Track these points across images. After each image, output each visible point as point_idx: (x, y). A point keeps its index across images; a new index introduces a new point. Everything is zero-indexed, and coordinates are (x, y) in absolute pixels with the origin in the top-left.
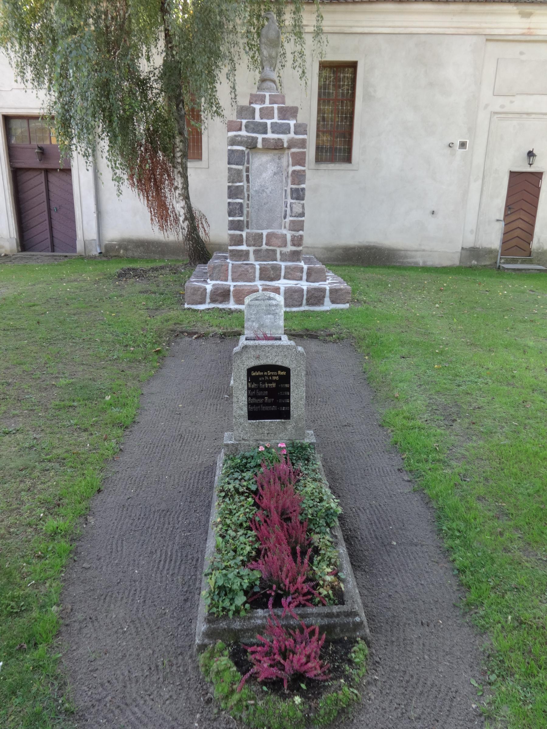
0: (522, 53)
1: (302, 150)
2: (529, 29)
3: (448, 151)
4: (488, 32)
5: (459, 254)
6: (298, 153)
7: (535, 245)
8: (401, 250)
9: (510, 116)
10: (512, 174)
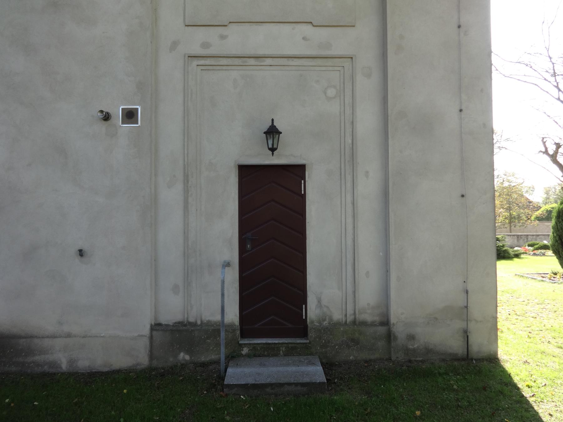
3: (102, 127)
5: (146, 341)
7: (312, 311)
8: (20, 337)
10: (247, 173)
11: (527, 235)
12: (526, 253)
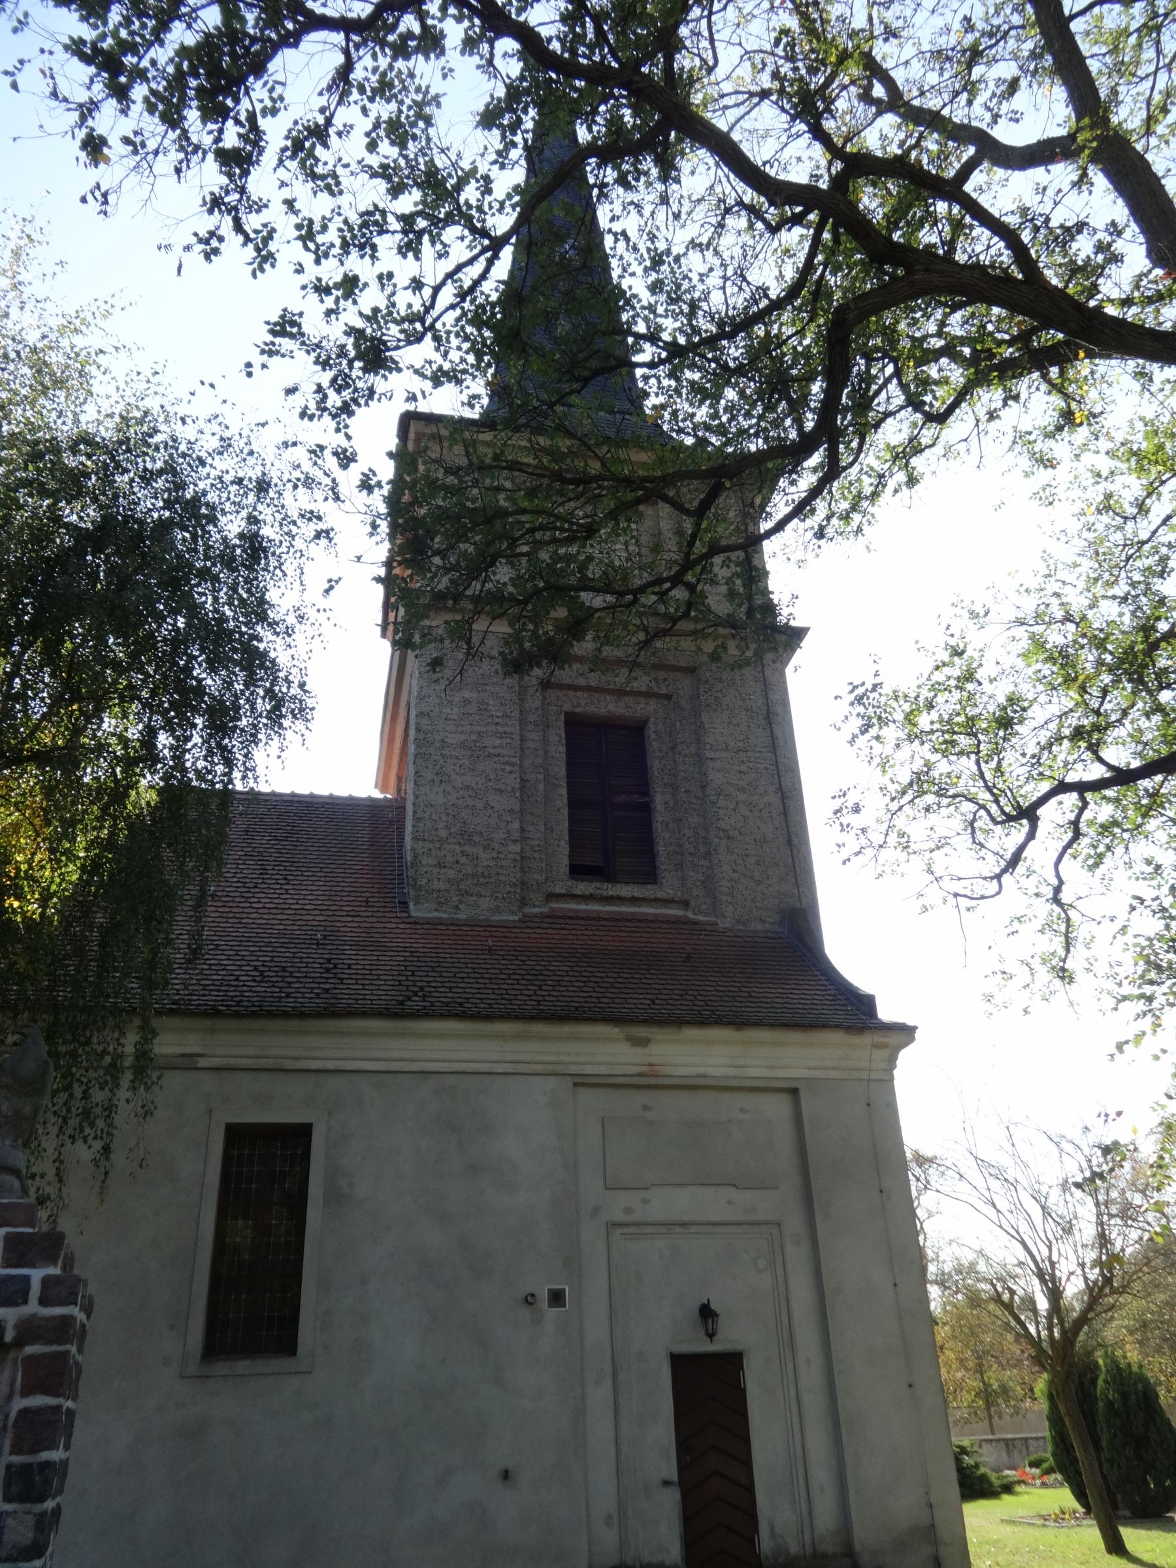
0: (646, 1108)
1: (55, 1348)
2: (650, 1065)
4: (574, 1069)
6: (43, 1356)
7: (765, 1543)
9: (648, 1230)
10: (680, 1363)
11: (1026, 1439)
12: (1024, 1482)
